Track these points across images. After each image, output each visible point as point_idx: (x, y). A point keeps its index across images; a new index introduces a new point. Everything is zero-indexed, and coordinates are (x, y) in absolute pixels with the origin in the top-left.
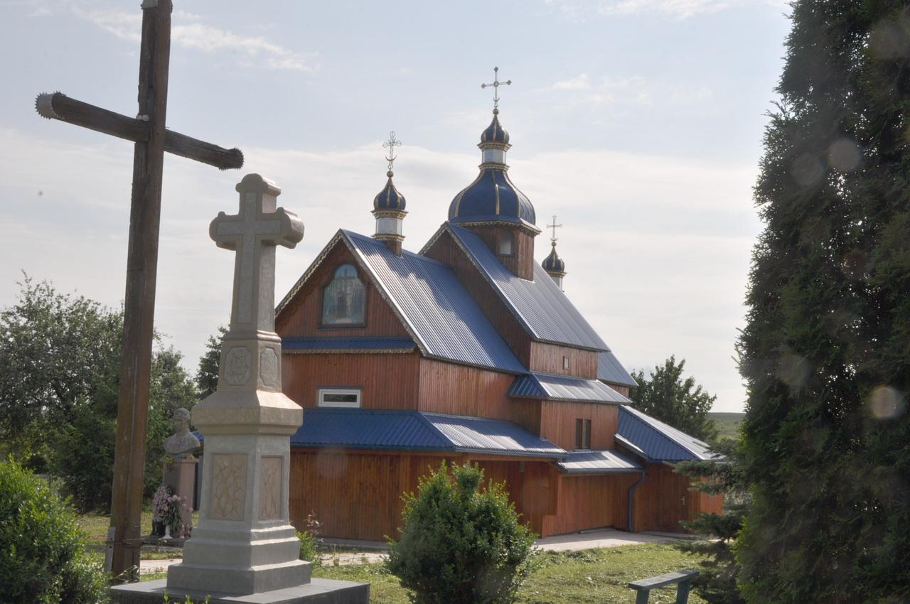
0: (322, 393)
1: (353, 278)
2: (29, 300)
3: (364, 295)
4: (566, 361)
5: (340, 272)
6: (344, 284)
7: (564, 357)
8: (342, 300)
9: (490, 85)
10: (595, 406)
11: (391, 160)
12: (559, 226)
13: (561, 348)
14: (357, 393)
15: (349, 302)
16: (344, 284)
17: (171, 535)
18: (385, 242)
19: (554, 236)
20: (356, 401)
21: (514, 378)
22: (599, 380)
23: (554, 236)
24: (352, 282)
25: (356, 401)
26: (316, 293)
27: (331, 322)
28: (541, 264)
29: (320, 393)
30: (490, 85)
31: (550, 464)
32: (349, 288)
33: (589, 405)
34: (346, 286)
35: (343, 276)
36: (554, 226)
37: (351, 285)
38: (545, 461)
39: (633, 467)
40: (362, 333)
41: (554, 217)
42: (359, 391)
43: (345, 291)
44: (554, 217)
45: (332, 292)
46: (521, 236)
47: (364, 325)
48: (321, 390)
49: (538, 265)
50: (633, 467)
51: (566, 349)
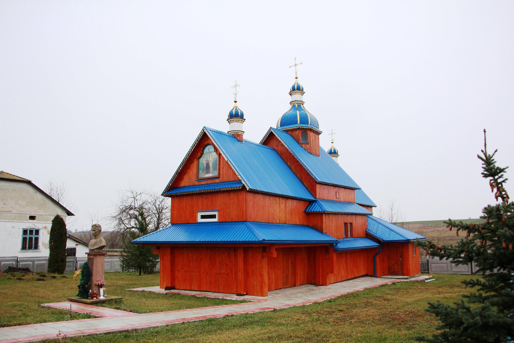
0: (200, 214)
1: (212, 152)
2: (144, 208)
3: (218, 160)
4: (337, 194)
5: (206, 150)
6: (208, 156)
7: (336, 192)
8: (208, 165)
9: (293, 66)
10: (354, 216)
11: (236, 94)
12: (334, 134)
13: (334, 188)
14: (216, 213)
15: (211, 165)
16: (208, 156)
17: (104, 296)
18: (233, 135)
19: (332, 138)
20: (216, 218)
21: (308, 203)
22: (356, 203)
23: (332, 138)
24: (212, 154)
25: (216, 218)
26: (195, 162)
27: (203, 177)
28: (327, 152)
29: (199, 214)
30: (293, 66)
31: (329, 247)
32: (211, 158)
33: (351, 216)
34: (209, 157)
35: (208, 152)
36: (332, 134)
37: (212, 156)
38: (327, 245)
39: (379, 245)
40: (217, 181)
41: (332, 130)
42: (217, 212)
43: (209, 159)
44: (332, 130)
45: (203, 161)
46: (311, 135)
47: (218, 177)
48: (199, 213)
49: (326, 152)
50: (379, 245)
51: (337, 188)
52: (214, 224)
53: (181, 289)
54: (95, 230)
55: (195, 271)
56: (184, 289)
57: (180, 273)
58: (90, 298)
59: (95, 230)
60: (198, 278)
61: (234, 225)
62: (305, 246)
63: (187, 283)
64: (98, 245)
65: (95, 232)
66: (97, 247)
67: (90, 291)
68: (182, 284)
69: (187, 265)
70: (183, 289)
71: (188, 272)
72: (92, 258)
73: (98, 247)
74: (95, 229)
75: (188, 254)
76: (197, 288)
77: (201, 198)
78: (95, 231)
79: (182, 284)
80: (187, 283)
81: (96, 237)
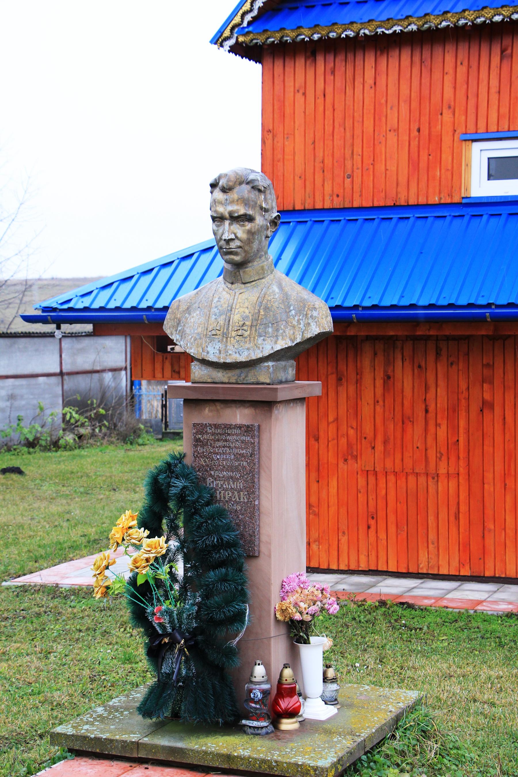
48: (476, 147)
52: (505, 210)
53: (343, 567)
54: (250, 219)
55: (443, 471)
56: (363, 566)
57: (334, 483)
58: (264, 724)
59: (250, 219)
60: (463, 508)
61: (439, 223)
62: (367, 334)
63: (382, 535)
64: (289, 332)
65: (250, 232)
66: (281, 344)
67: (259, 671)
68: (344, 539)
69: (380, 438)
70: (353, 567)
71: (392, 478)
72: (248, 429)
73: (288, 343)
74: (250, 212)
75: (387, 378)
76: (455, 563)
77: (496, 59)
78: (248, 226)
79: (344, 539)
80: (382, 535)
81: (251, 271)
